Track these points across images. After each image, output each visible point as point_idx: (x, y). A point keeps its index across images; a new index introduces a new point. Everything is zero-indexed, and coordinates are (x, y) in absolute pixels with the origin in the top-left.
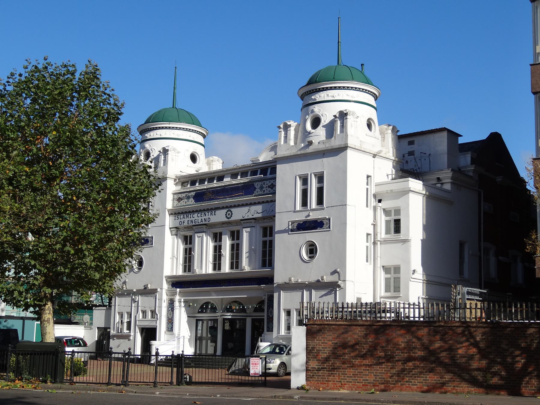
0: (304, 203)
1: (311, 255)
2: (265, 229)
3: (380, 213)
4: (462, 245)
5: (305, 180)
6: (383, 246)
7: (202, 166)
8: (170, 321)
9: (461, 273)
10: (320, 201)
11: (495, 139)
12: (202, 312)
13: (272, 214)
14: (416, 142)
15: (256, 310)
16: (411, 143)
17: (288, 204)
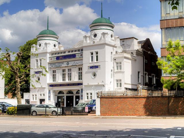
0: (92, 60)
1: (95, 76)
2: (79, 69)
3: (115, 64)
4: (139, 72)
5: (92, 54)
6: (116, 74)
7: (57, 49)
8: (49, 97)
9: (138, 81)
10: (97, 60)
11: (148, 41)
12: (59, 94)
13: (82, 64)
14: (125, 41)
15: (77, 93)
16: (123, 41)
17: (87, 60)
